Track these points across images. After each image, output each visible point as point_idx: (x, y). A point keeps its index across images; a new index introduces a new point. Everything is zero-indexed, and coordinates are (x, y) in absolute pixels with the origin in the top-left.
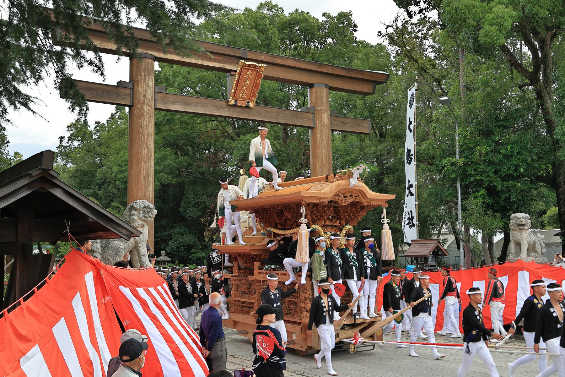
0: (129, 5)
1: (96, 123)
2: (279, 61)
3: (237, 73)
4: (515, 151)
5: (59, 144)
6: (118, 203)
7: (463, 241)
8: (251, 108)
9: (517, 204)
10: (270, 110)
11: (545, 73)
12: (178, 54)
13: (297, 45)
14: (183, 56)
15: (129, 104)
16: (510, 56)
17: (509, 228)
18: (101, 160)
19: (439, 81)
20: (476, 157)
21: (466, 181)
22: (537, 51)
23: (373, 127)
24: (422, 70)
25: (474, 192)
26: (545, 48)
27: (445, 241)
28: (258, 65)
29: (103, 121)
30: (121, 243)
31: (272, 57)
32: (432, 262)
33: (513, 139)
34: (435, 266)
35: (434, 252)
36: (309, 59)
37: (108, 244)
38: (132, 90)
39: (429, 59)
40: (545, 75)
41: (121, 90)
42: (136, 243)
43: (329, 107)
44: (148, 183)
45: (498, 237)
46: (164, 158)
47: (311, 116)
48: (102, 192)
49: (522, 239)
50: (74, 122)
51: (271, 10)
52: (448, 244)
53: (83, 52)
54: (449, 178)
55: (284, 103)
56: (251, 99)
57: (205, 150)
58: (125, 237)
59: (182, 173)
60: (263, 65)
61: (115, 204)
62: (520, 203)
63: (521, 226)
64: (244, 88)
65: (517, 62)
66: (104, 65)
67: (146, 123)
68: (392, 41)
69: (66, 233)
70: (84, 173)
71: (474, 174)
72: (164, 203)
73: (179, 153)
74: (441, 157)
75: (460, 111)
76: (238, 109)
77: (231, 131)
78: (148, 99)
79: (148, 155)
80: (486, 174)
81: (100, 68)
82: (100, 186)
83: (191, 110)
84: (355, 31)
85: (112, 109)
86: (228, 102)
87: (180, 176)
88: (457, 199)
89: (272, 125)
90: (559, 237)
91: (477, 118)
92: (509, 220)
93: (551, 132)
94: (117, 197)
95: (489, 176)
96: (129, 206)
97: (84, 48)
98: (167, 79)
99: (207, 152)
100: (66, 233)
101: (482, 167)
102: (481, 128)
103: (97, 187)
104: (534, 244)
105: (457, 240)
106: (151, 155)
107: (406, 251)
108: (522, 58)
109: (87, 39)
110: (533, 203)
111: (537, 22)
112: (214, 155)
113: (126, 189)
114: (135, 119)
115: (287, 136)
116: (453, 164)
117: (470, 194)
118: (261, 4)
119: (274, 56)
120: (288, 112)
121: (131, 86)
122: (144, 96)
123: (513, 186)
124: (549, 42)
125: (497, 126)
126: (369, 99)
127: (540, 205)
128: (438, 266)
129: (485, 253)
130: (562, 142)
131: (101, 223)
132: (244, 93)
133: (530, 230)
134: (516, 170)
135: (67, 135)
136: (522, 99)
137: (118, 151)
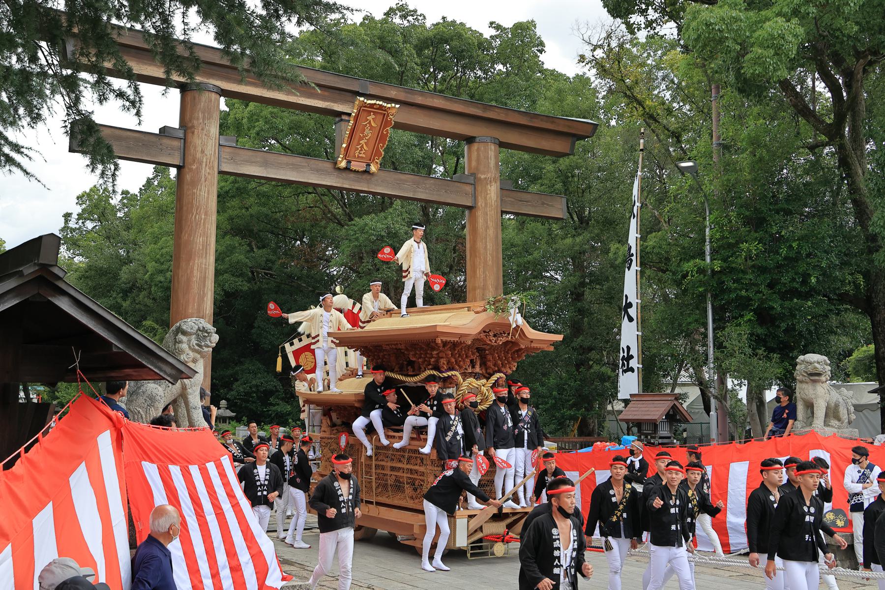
2: (419, 100)
4: (804, 254)
5: (63, 225)
6: (153, 321)
7: (716, 397)
8: (373, 174)
9: (806, 339)
11: (854, 126)
16: (796, 98)
18: (128, 252)
19: (677, 136)
20: (739, 260)
21: (722, 299)
24: (651, 117)
26: (854, 85)
28: (385, 105)
30: (159, 388)
31: (408, 93)
32: (664, 431)
33: (799, 233)
34: (669, 438)
36: (465, 97)
37: (139, 388)
38: (182, 141)
40: (853, 130)
41: (166, 141)
45: (770, 395)
46: (231, 250)
47: (469, 188)
48: (128, 302)
51: (405, 18)
52: (689, 401)
54: (693, 294)
55: (423, 167)
58: (168, 378)
60: (393, 105)
61: (148, 323)
62: (812, 336)
63: (814, 376)
66: (142, 99)
68: (603, 71)
70: (101, 272)
71: (736, 289)
74: (681, 260)
75: (712, 186)
76: (352, 175)
78: (209, 156)
79: (206, 246)
80: (756, 289)
81: (134, 104)
82: (126, 293)
84: (541, 51)
86: (336, 163)
88: (706, 329)
95: (759, 292)
96: (174, 328)
99: (299, 242)
100: (74, 369)
103: (121, 295)
104: (837, 406)
105: (703, 393)
108: (814, 100)
110: (832, 337)
111: (842, 43)
114: (186, 187)
116: (701, 271)
118: (391, 9)
119: (412, 91)
121: (182, 136)
122: (203, 152)
125: (774, 210)
126: (564, 163)
128: (674, 438)
131: (131, 354)
132: (363, 147)
134: (805, 282)
135: (76, 210)
136: (814, 166)
137: (156, 239)
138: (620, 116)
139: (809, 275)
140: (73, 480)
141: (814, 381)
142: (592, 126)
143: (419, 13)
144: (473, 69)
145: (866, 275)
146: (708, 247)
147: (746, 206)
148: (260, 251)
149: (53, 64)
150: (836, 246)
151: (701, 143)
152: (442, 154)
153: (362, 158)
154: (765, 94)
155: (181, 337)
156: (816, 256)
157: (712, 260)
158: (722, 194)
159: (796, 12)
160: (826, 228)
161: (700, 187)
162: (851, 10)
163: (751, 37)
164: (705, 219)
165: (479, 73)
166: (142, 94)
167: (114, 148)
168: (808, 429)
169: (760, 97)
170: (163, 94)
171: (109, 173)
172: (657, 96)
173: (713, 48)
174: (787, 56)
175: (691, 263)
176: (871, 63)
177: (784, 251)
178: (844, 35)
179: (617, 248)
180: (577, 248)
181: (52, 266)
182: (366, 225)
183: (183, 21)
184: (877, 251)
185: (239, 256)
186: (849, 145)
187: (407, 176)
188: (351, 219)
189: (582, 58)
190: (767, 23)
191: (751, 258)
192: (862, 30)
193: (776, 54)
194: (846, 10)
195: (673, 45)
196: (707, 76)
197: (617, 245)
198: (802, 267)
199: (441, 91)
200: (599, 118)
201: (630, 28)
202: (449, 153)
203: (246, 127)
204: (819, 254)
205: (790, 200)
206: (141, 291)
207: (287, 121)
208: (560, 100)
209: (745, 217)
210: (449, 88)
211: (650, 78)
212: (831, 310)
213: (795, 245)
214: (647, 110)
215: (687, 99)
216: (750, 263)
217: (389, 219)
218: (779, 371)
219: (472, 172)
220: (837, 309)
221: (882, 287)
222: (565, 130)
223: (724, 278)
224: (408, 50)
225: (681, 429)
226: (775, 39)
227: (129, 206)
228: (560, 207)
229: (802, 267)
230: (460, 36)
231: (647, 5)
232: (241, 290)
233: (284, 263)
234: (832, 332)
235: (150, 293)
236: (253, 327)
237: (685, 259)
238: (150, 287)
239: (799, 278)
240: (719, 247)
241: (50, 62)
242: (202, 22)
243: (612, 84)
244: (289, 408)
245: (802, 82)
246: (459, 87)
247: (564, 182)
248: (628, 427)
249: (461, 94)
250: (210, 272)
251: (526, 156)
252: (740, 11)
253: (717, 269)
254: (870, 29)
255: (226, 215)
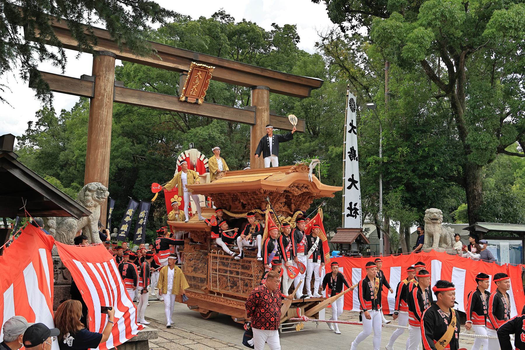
0: (90, 8)
1: (62, 111)
2: (226, 64)
3: (189, 73)
4: (431, 153)
5: (27, 128)
6: (77, 183)
7: (383, 231)
8: (200, 105)
9: (431, 200)
10: (216, 107)
11: (459, 86)
12: (133, 53)
13: (244, 50)
14: (137, 55)
15: (91, 96)
16: (430, 70)
17: (424, 222)
18: (64, 144)
19: (367, 89)
20: (397, 157)
21: (388, 178)
22: (453, 66)
23: (307, 126)
24: (353, 78)
25: (395, 188)
26: (460, 65)
27: (367, 230)
28: (207, 67)
29: (69, 109)
30: (75, 221)
31: (220, 60)
32: (354, 248)
33: (430, 142)
34: (357, 252)
35: (356, 240)
36: (254, 64)
37: (63, 221)
38: (94, 83)
39: (360, 70)
40: (460, 88)
41: (84, 83)
42: (89, 221)
43: (269, 107)
44: (103, 167)
45: (413, 229)
46: (122, 144)
47: (252, 114)
48: (63, 172)
49: (435, 232)
50: (42, 109)
51: (224, 19)
52: (370, 232)
53: (48, 47)
54: (372, 175)
55: (230, 101)
56: (200, 97)
57: (158, 139)
58: (75, 216)
59: (137, 159)
60: (212, 67)
61: (74, 184)
62: (434, 199)
63: (434, 220)
64: (194, 87)
65: (435, 75)
66: (66, 59)
67: (105, 113)
68: (328, 52)
69: (23, 209)
70: (49, 155)
71: (395, 172)
72: (119, 186)
73: (135, 141)
74: (366, 156)
75: (384, 116)
76: (188, 105)
77: (182, 124)
78: (108, 92)
79: (105, 142)
80: (405, 172)
81: (61, 62)
82: (62, 167)
83: (146, 103)
84: (297, 42)
85: (77, 99)
86: (179, 98)
87: (135, 161)
88: (379, 194)
89: (219, 121)
90: (467, 231)
91: (399, 123)
92: (424, 214)
93: (463, 138)
94: (77, 178)
95: (407, 174)
96: (84, 187)
97: (49, 43)
98: (128, 75)
99: (160, 141)
100: (23, 209)
101: (402, 166)
102: (402, 132)
103: (60, 168)
104: (446, 236)
105: (378, 229)
106: (107, 142)
107: (332, 237)
108: (439, 72)
109: (51, 34)
110: (445, 200)
111: (454, 41)
112: (166, 144)
113: (84, 171)
114: (95, 109)
115: (232, 131)
116: (377, 162)
117: (390, 190)
118: (216, 13)
119: (222, 60)
120: (232, 109)
121: (93, 80)
122: (105, 89)
123: (428, 184)
124: (463, 59)
125: (416, 130)
126: (306, 101)
127: (452, 202)
128: (360, 252)
129: (402, 243)
130: (473, 147)
131: (54, 202)
132: (194, 90)
133: (443, 224)
134: (431, 169)
135: (35, 120)
136: (438, 108)
137: (80, 137)
138: (337, 77)
139: (434, 166)
140: (25, 272)
141: (434, 223)
142: (320, 82)
143: (231, 16)
144: (258, 49)
145: (464, 166)
146: (381, 150)
147: (402, 128)
148: (138, 145)
149: (14, 38)
150: (448, 151)
151: (379, 94)
152: (241, 95)
153: (194, 95)
154: (413, 67)
155: (88, 192)
156: (437, 155)
157: (382, 156)
158: (389, 120)
159: (429, 24)
160: (443, 141)
161: (377, 116)
162: (459, 24)
163: (406, 37)
164: (380, 134)
165: (262, 50)
166: (66, 56)
167: (50, 85)
168: (430, 249)
169: (410, 69)
170: (77, 58)
171: (48, 99)
172: (356, 66)
173: (387, 42)
174: (425, 48)
175: (371, 158)
176: (469, 53)
177: (420, 152)
178: (455, 38)
179: (333, 149)
180: (312, 148)
181: (10, 152)
182: (197, 132)
183: (88, 18)
184: (470, 154)
185: (126, 148)
186: (456, 97)
187: (220, 106)
188: (189, 129)
189: (317, 44)
190: (415, 30)
191: (403, 156)
192: (464, 35)
193: (420, 46)
194: (456, 23)
195: (366, 39)
196: (384, 57)
197: (333, 147)
198: (430, 162)
199: (241, 60)
200: (325, 77)
201: (343, 29)
202: (245, 94)
203: (132, 76)
204: (439, 154)
205: (424, 125)
206: (71, 166)
207: (156, 73)
208: (305, 67)
209: (401, 134)
210: (246, 58)
211: (354, 56)
212: (445, 185)
213: (426, 149)
214: (351, 74)
215: (373, 68)
216: (403, 158)
217: (210, 130)
218: (416, 217)
219: (254, 105)
220: (448, 184)
221: (472, 173)
222: (306, 84)
223: (389, 166)
224: (223, 37)
225: (366, 247)
226: (419, 38)
227: (65, 118)
228: (302, 125)
229: (430, 162)
230: (253, 30)
231: (352, 17)
232: (127, 167)
233: (151, 152)
234: (445, 196)
235: (76, 167)
236: (133, 188)
237: (369, 155)
238: (76, 164)
239: (428, 167)
240: (387, 150)
241: (13, 37)
242: (100, 18)
243: (332, 59)
244: (152, 233)
245: (434, 62)
246: (251, 57)
247: (305, 112)
248: (337, 246)
249: (252, 62)
250: (108, 157)
251: (286, 97)
252: (401, 22)
253: (385, 161)
254: (468, 35)
255: (120, 125)
